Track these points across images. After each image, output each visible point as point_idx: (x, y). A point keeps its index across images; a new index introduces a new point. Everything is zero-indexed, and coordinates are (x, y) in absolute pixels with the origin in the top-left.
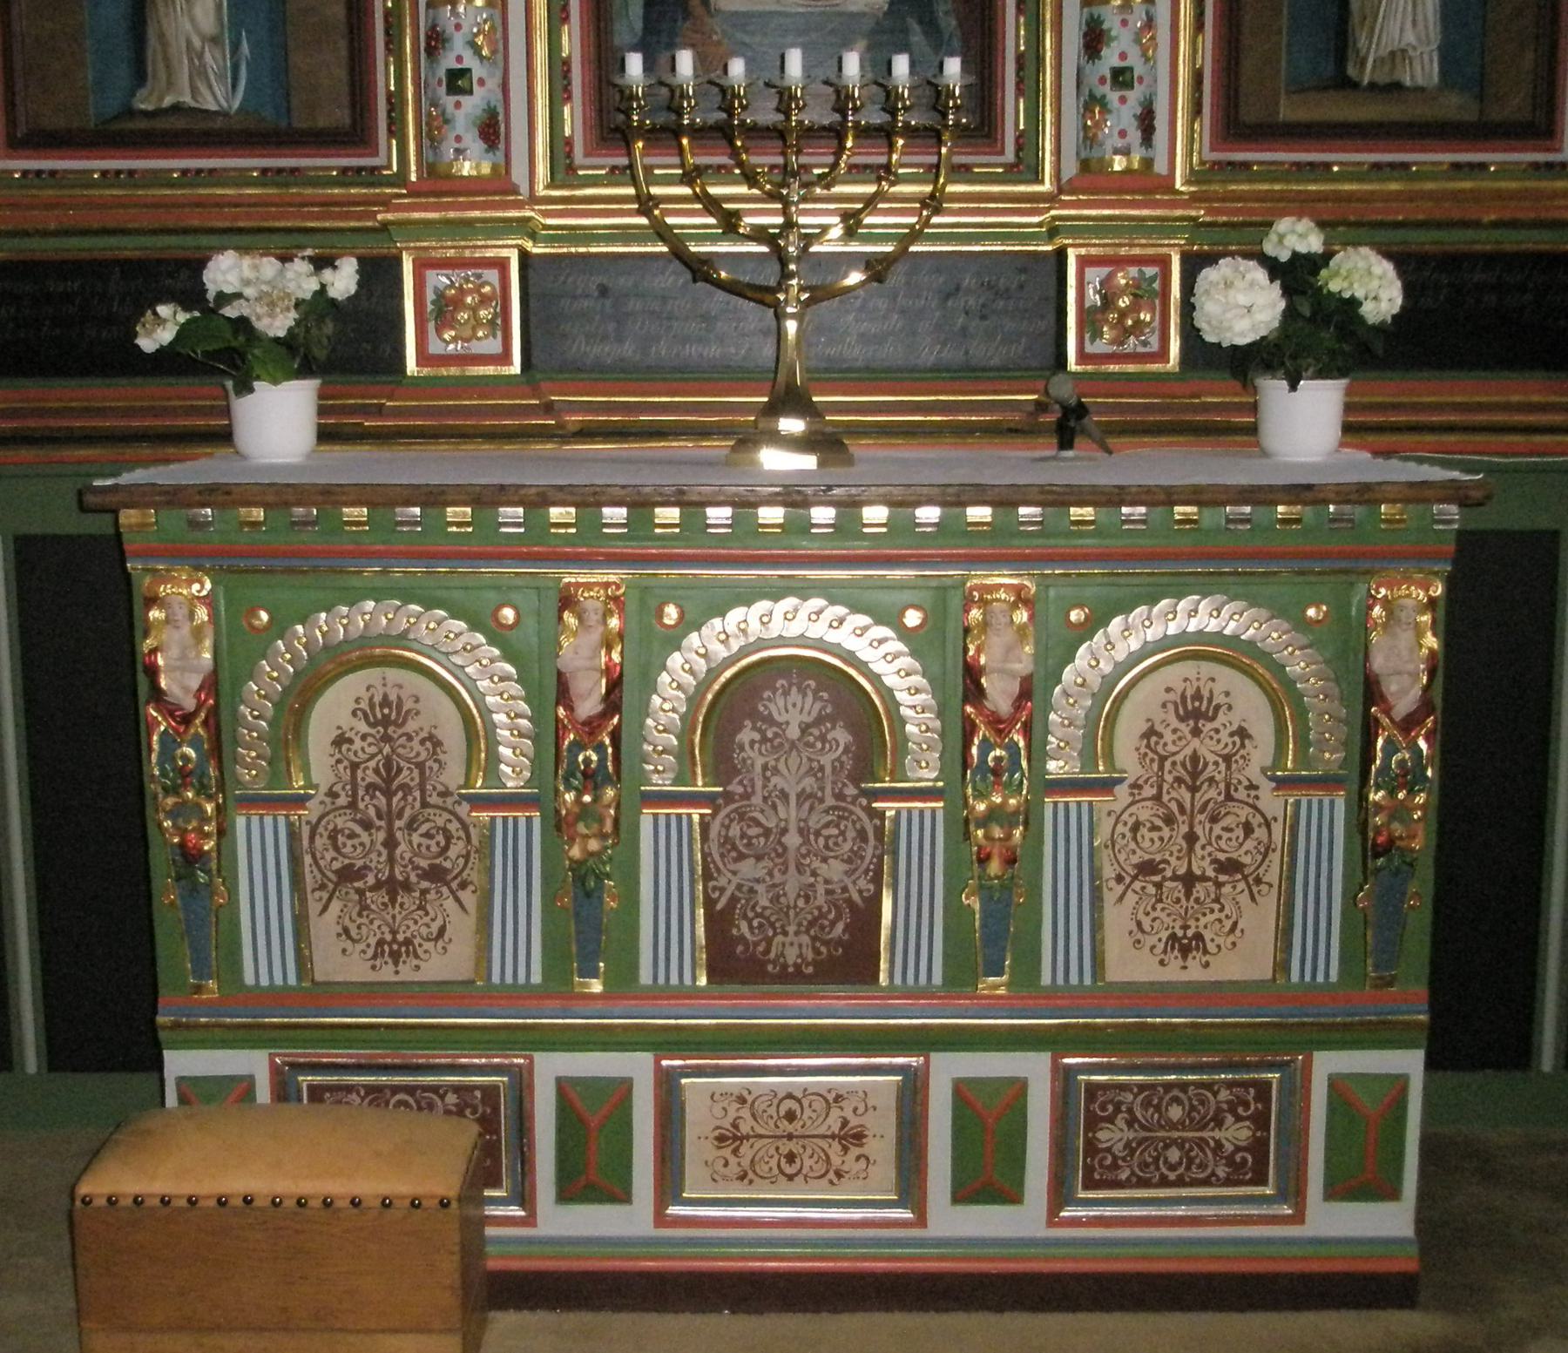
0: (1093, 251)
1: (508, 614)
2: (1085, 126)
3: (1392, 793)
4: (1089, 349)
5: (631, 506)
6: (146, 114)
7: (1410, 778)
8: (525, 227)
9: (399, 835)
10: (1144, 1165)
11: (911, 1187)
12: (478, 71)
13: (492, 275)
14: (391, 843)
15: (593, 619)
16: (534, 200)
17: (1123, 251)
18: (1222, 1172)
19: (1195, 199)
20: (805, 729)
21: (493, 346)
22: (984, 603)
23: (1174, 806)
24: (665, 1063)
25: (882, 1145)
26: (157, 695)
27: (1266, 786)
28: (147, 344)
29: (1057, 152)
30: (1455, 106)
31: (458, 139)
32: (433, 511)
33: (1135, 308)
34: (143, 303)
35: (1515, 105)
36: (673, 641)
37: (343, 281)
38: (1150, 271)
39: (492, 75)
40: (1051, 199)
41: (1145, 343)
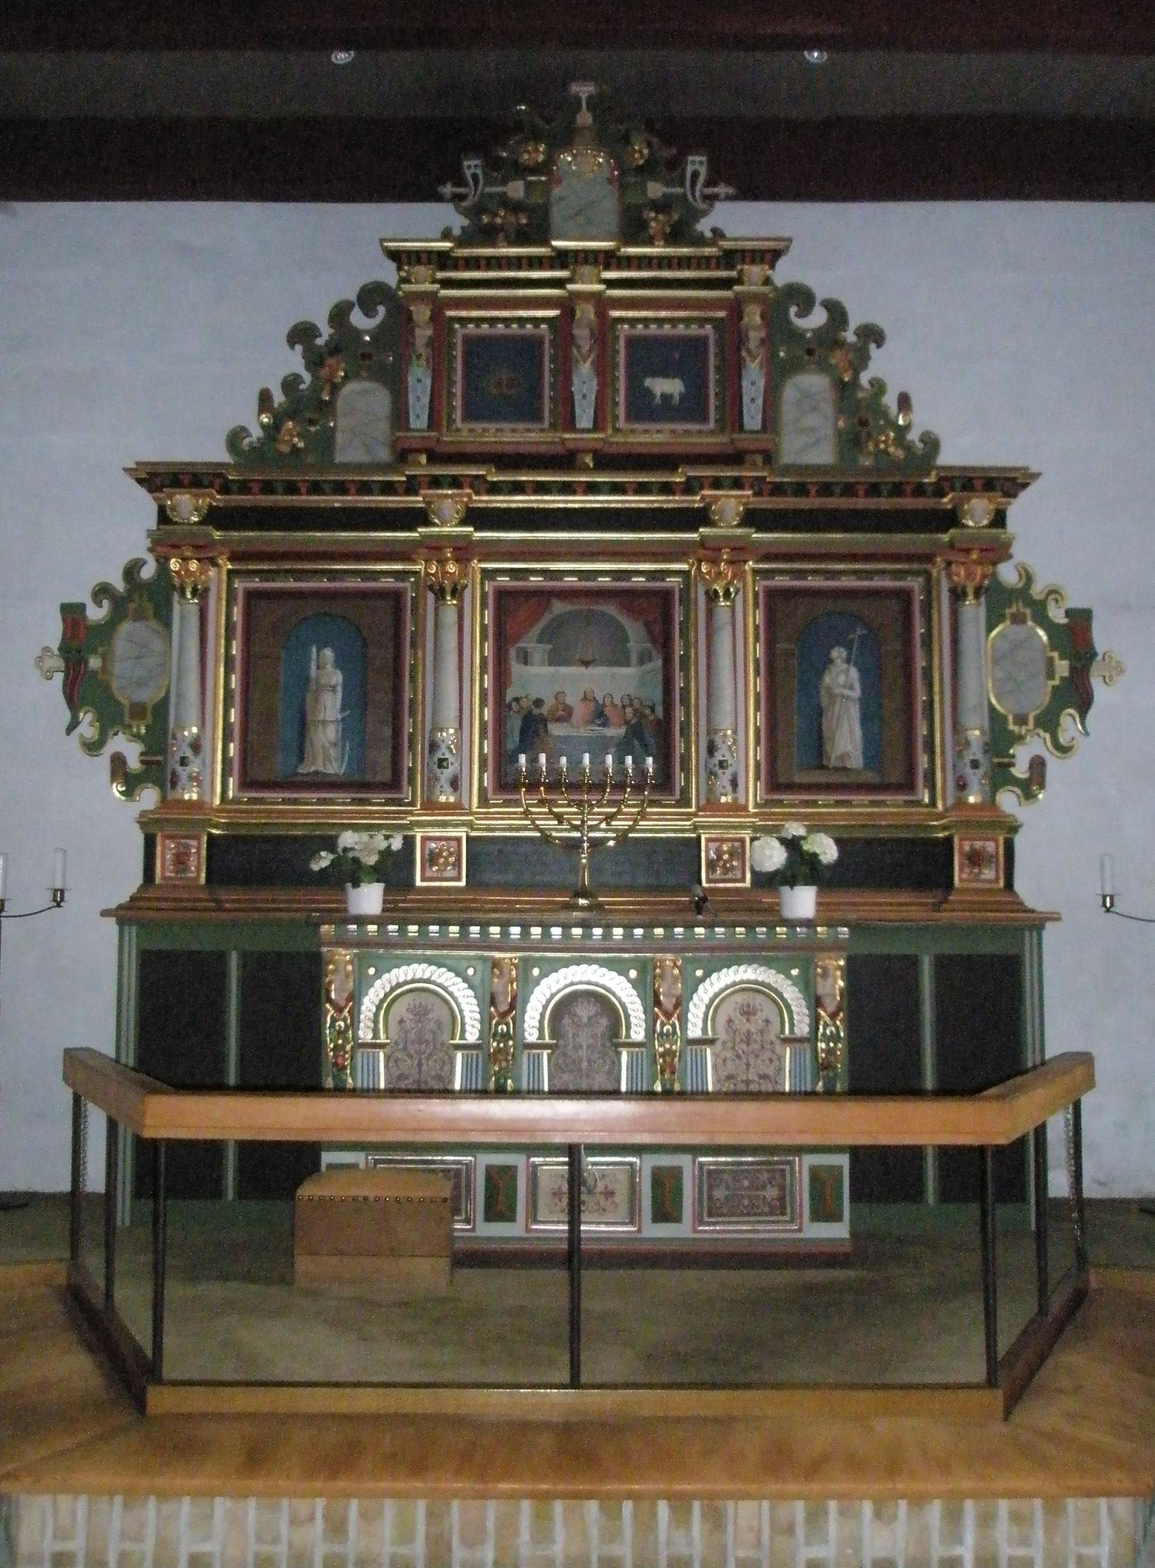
0: (712, 836)
1: (471, 971)
2: (708, 784)
3: (828, 1044)
4: (711, 877)
5: (521, 926)
6: (303, 775)
7: (835, 1038)
9: (423, 1061)
10: (733, 1207)
12: (451, 759)
13: (454, 843)
14: (420, 1065)
15: (506, 971)
16: (472, 814)
17: (725, 836)
18: (767, 1209)
19: (755, 815)
20: (590, 1019)
21: (453, 874)
22: (661, 967)
23: (740, 1051)
25: (622, 1197)
26: (330, 1000)
27: (778, 1043)
28: (316, 866)
29: (698, 796)
30: (871, 777)
31: (442, 787)
32: (444, 928)
34: (314, 853)
35: (896, 776)
36: (537, 983)
37: (397, 844)
38: (737, 844)
39: (456, 760)
40: (695, 815)
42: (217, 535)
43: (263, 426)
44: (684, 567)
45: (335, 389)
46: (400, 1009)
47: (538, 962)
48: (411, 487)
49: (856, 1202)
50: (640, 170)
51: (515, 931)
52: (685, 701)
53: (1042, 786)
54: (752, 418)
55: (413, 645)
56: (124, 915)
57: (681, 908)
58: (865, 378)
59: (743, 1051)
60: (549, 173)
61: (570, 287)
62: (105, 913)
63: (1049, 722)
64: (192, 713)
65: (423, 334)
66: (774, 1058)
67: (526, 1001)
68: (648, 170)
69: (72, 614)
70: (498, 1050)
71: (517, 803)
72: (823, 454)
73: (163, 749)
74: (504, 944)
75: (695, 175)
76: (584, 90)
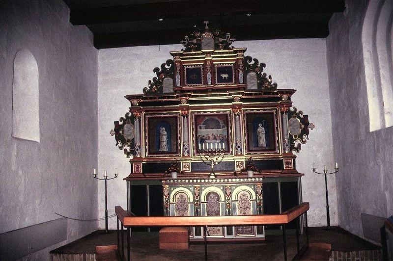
7: (261, 199)
8: (191, 160)
11: (223, 234)
24: (149, 229)
30: (267, 148)
42: (142, 107)
43: (149, 87)
44: (230, 110)
45: (162, 80)
46: (178, 196)
48: (177, 97)
49: (267, 229)
50: (218, 36)
51: (187, 181)
52: (231, 135)
53: (300, 149)
54: (241, 81)
55: (180, 126)
56: (127, 179)
57: (232, 175)
58: (262, 73)
60: (201, 38)
61: (206, 58)
62: (124, 179)
63: (301, 137)
64: (138, 141)
65: (178, 68)
67: (201, 193)
68: (220, 36)
69: (116, 123)
70: (197, 204)
71: (199, 155)
72: (255, 88)
73: (134, 148)
74: (197, 183)
75: (228, 37)
76: (207, 22)
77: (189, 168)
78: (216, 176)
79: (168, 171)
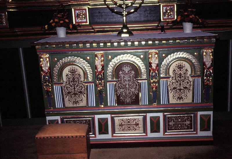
1: (88, 58)
7: (210, 75)
8: (88, 4)
9: (75, 87)
11: (145, 131)
14: (75, 88)
17: (168, 4)
20: (128, 71)
21: (85, 20)
23: (178, 80)
27: (190, 77)
33: (170, 12)
41: (172, 17)
46: (66, 71)
47: (110, 54)
59: (72, 84)
66: (189, 82)
77: (85, 17)
78: (130, 32)
79: (50, 25)
